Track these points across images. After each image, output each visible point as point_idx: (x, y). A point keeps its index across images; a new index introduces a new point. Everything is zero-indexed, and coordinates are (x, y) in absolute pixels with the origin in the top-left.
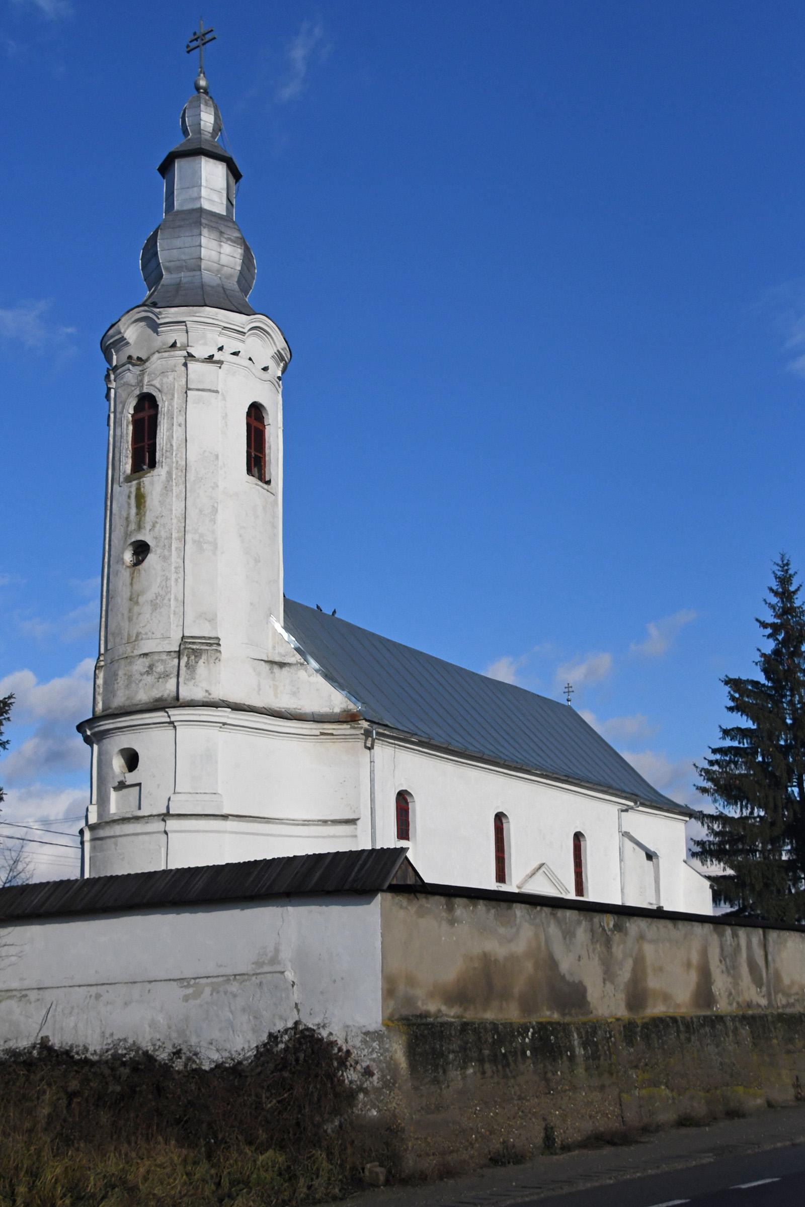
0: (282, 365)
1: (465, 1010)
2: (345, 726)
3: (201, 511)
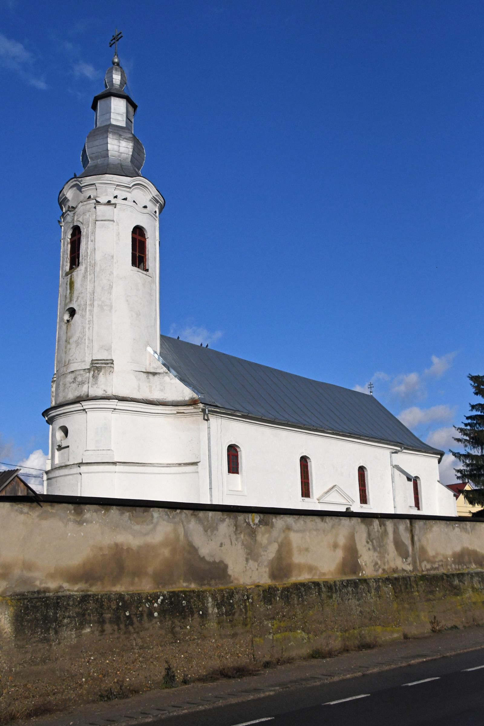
0: (158, 205)
1: (91, 585)
2: (191, 407)
3: (103, 288)
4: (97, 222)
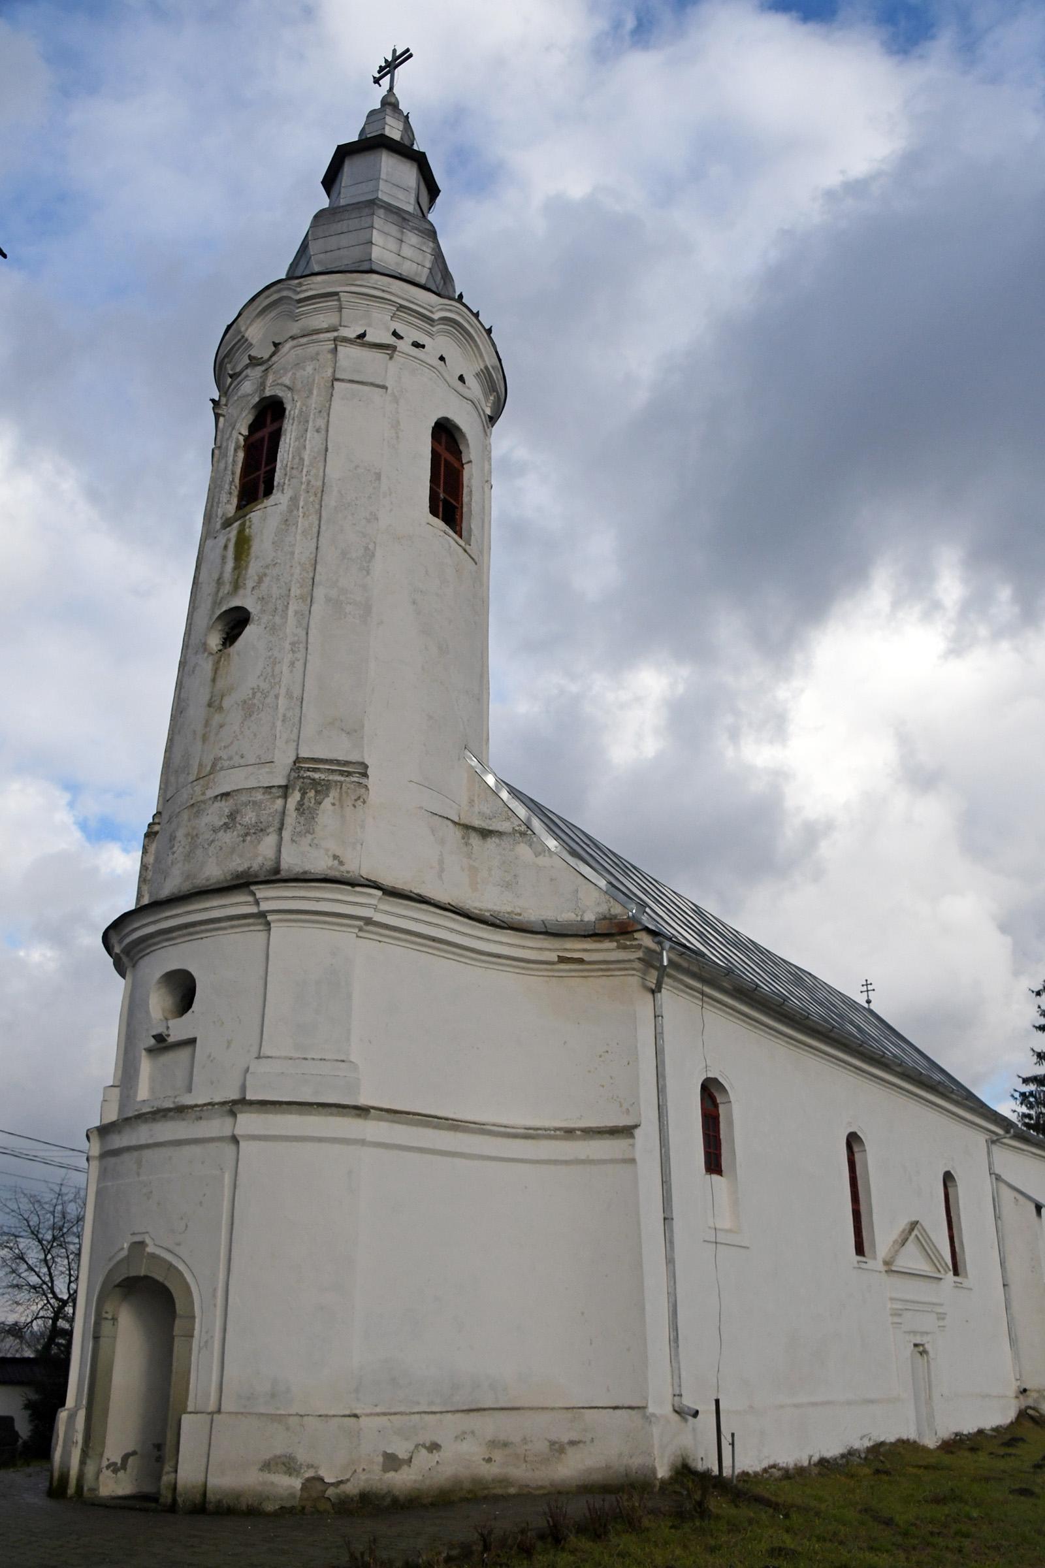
3: (344, 554)
4: (336, 383)
